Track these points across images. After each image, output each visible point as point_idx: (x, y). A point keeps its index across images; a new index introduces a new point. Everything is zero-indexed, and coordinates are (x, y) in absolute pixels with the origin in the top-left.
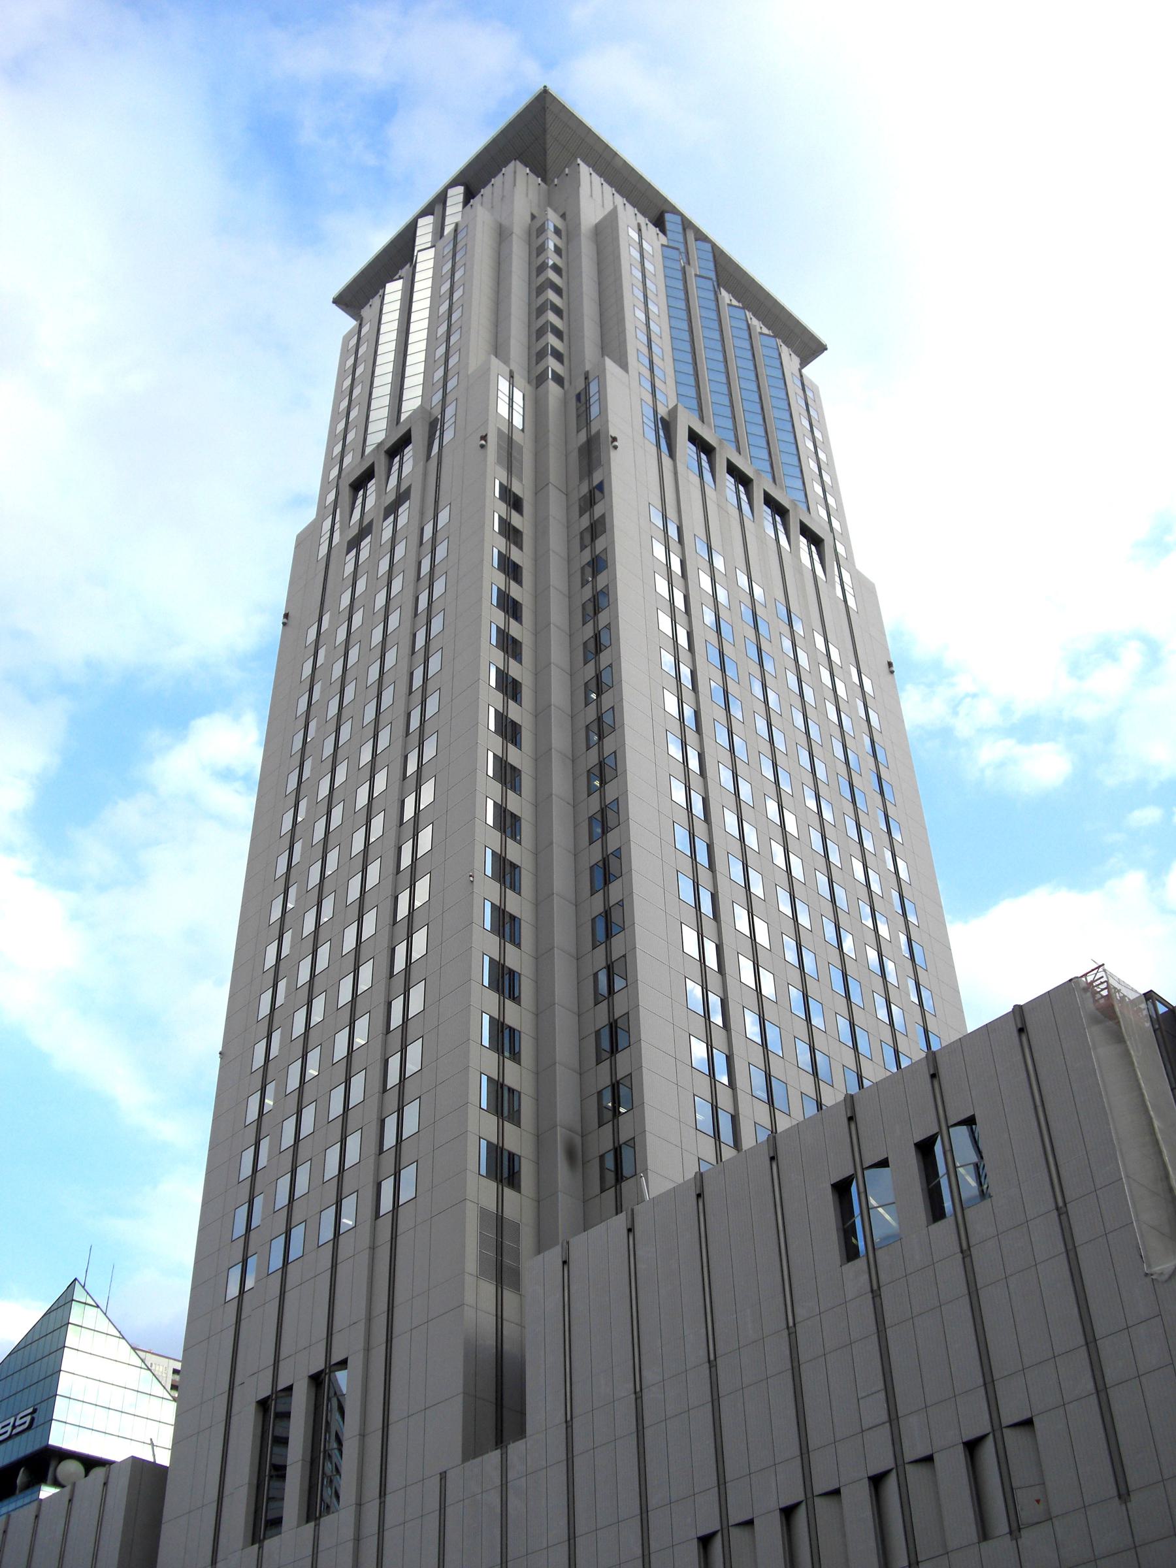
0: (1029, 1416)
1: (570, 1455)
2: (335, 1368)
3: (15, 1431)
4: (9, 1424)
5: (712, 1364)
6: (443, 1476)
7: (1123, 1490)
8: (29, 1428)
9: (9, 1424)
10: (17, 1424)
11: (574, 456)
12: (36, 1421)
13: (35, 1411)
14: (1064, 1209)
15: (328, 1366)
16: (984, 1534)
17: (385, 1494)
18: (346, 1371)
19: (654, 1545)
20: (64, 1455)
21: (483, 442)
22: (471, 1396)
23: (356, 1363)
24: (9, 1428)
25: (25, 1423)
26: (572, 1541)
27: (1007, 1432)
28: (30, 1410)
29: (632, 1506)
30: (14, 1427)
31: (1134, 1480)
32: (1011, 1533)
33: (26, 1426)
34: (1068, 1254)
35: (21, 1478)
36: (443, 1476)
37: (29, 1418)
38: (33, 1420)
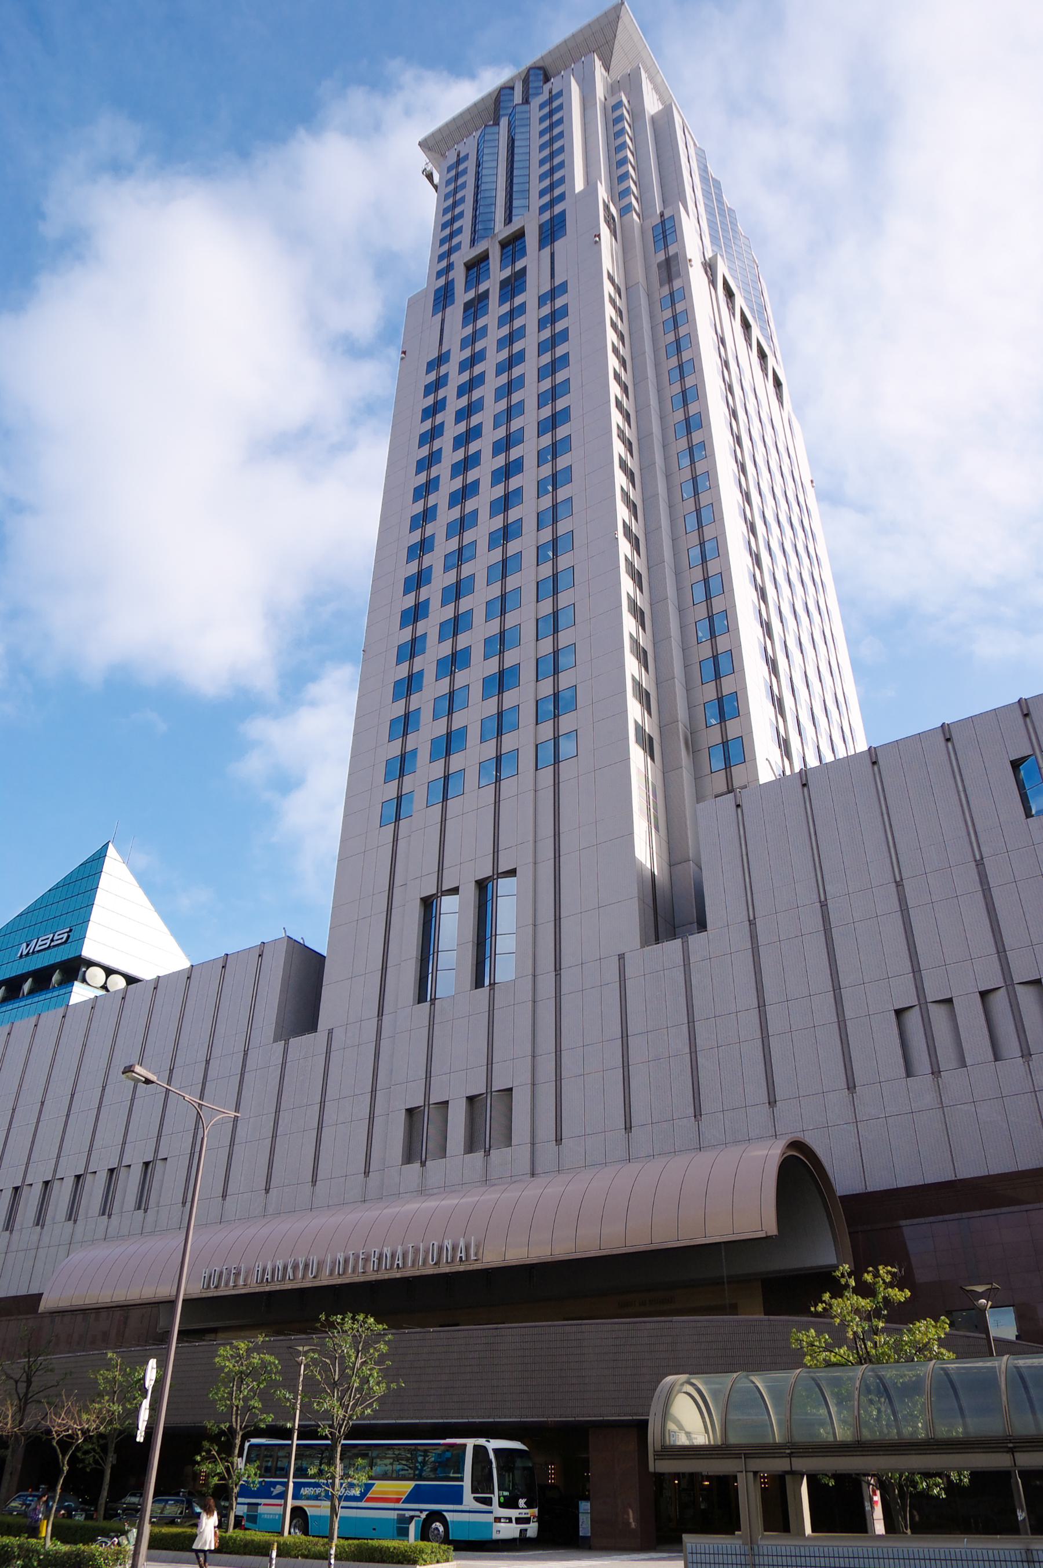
0: (511, 1086)
1: (378, 1039)
2: (502, 875)
3: (52, 944)
4: (48, 939)
5: (208, 1062)
6: (621, 957)
7: (772, 1100)
8: (66, 942)
9: (48, 939)
10: (54, 939)
11: (655, 269)
12: (71, 937)
13: (71, 931)
14: (901, 883)
15: (439, 891)
16: (909, 1073)
17: (382, 1015)
18: (515, 878)
19: (849, 1014)
20: (90, 964)
21: (403, 355)
22: (642, 900)
23: (525, 872)
24: (48, 941)
25: (62, 938)
26: (374, 1093)
27: (932, 1008)
28: (68, 930)
29: (615, 1029)
30: (52, 940)
31: (859, 1078)
32: (933, 1073)
33: (63, 940)
34: (753, 950)
35: (56, 977)
36: (621, 957)
37: (66, 935)
38: (68, 937)
